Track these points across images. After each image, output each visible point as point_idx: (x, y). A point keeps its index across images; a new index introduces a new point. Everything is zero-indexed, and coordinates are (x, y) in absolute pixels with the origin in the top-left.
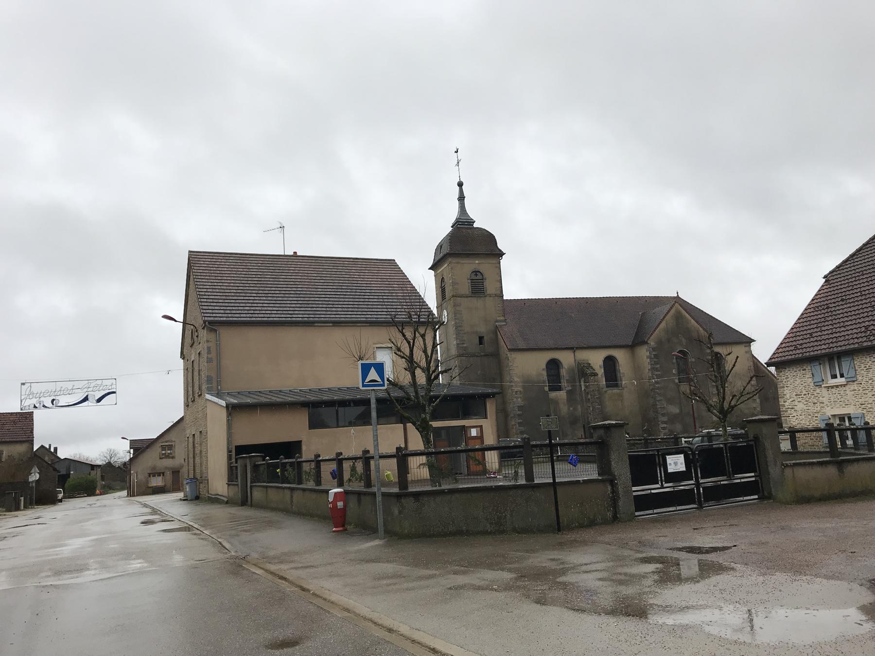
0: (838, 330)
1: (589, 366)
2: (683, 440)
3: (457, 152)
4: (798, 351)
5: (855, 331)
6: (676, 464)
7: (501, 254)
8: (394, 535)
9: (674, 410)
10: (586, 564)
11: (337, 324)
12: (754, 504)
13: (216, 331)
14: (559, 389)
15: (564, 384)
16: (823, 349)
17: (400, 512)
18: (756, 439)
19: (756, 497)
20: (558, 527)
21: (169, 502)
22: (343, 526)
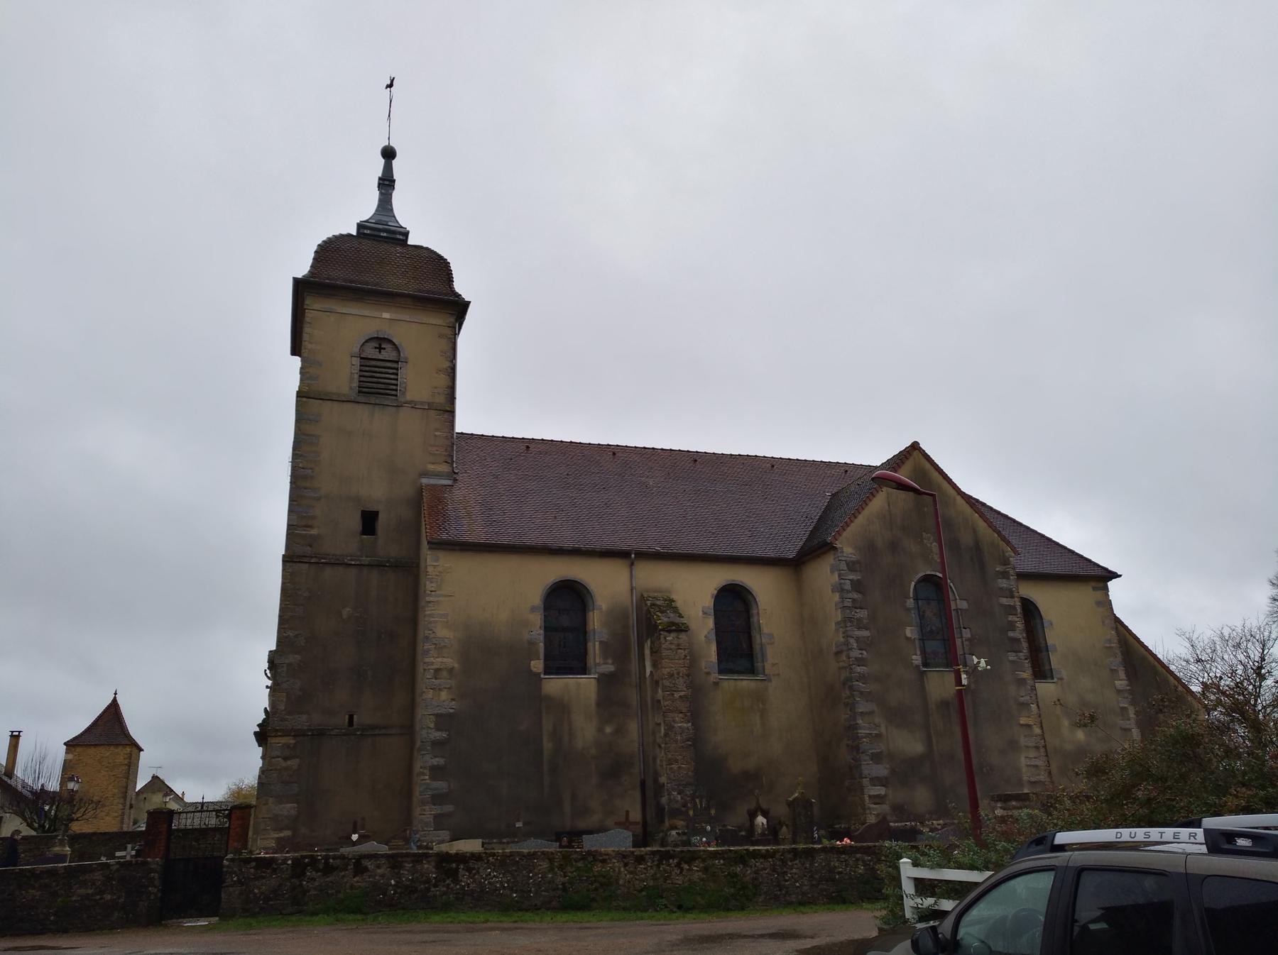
1: (670, 604)
2: (907, 869)
3: (390, 86)
9: (909, 744)
14: (584, 670)
15: (594, 648)
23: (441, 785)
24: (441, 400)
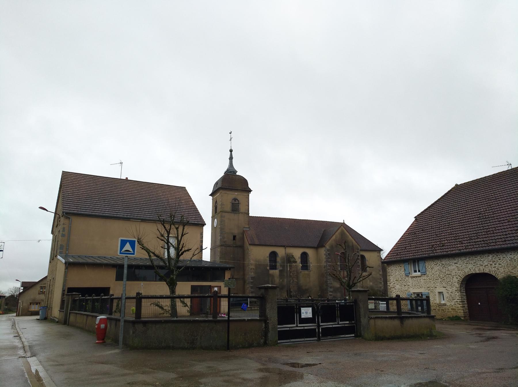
0: (419, 246)
4: (398, 256)
5: (427, 247)
6: (306, 313)
7: (250, 191)
8: (128, 347)
10: (226, 371)
11: (143, 220)
12: (352, 339)
13: (69, 218)
14: (276, 269)
15: (278, 264)
16: (410, 256)
17: (133, 333)
18: (356, 302)
19: (353, 335)
20: (228, 347)
21: (32, 320)
22: (103, 339)
23: (252, 290)
24: (247, 212)
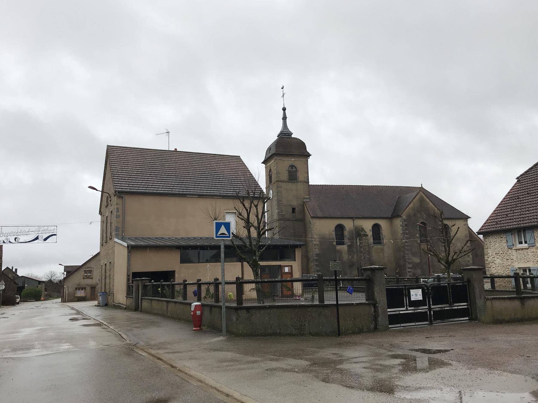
1: (363, 230)
3: (283, 88)
4: (498, 226)
6: (416, 295)
7: (309, 155)
8: (233, 334)
9: (417, 260)
10: (356, 358)
11: (201, 196)
12: (465, 323)
13: (122, 197)
14: (343, 244)
16: (514, 225)
17: (237, 319)
19: (467, 318)
20: (339, 333)
22: (200, 327)
